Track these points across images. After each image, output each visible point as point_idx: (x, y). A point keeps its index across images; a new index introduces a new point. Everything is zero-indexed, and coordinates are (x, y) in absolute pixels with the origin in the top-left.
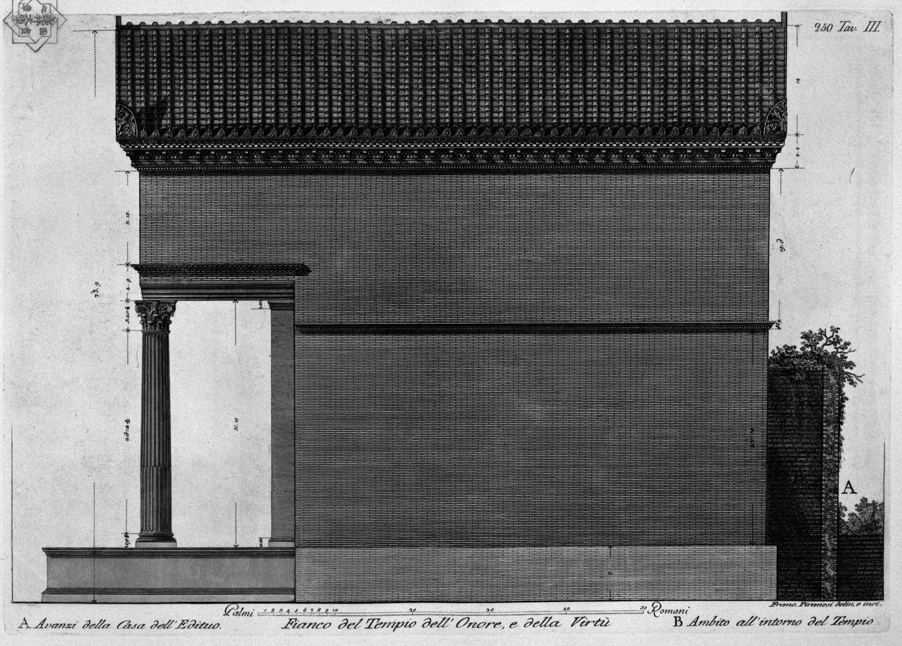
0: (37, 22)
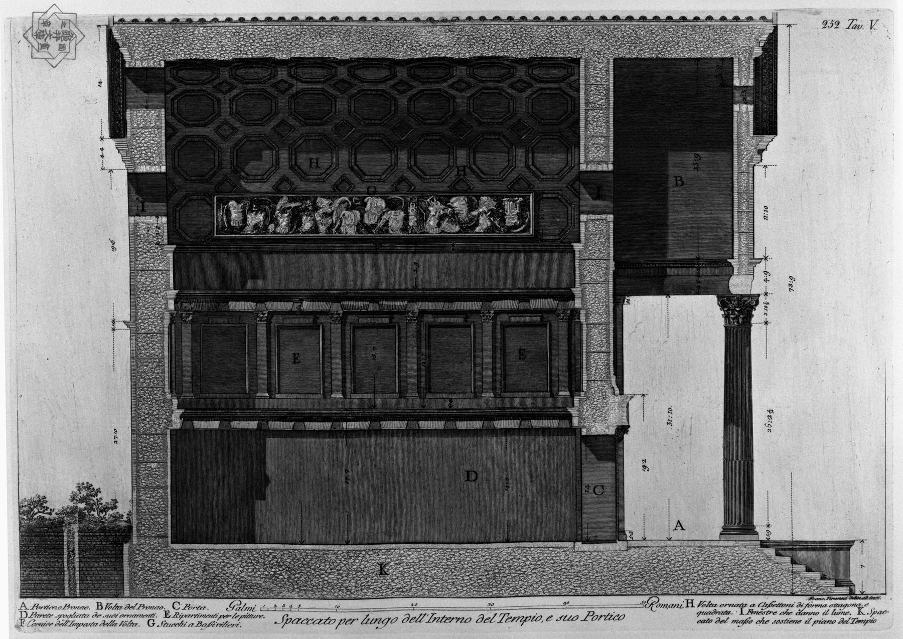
0: (56, 37)
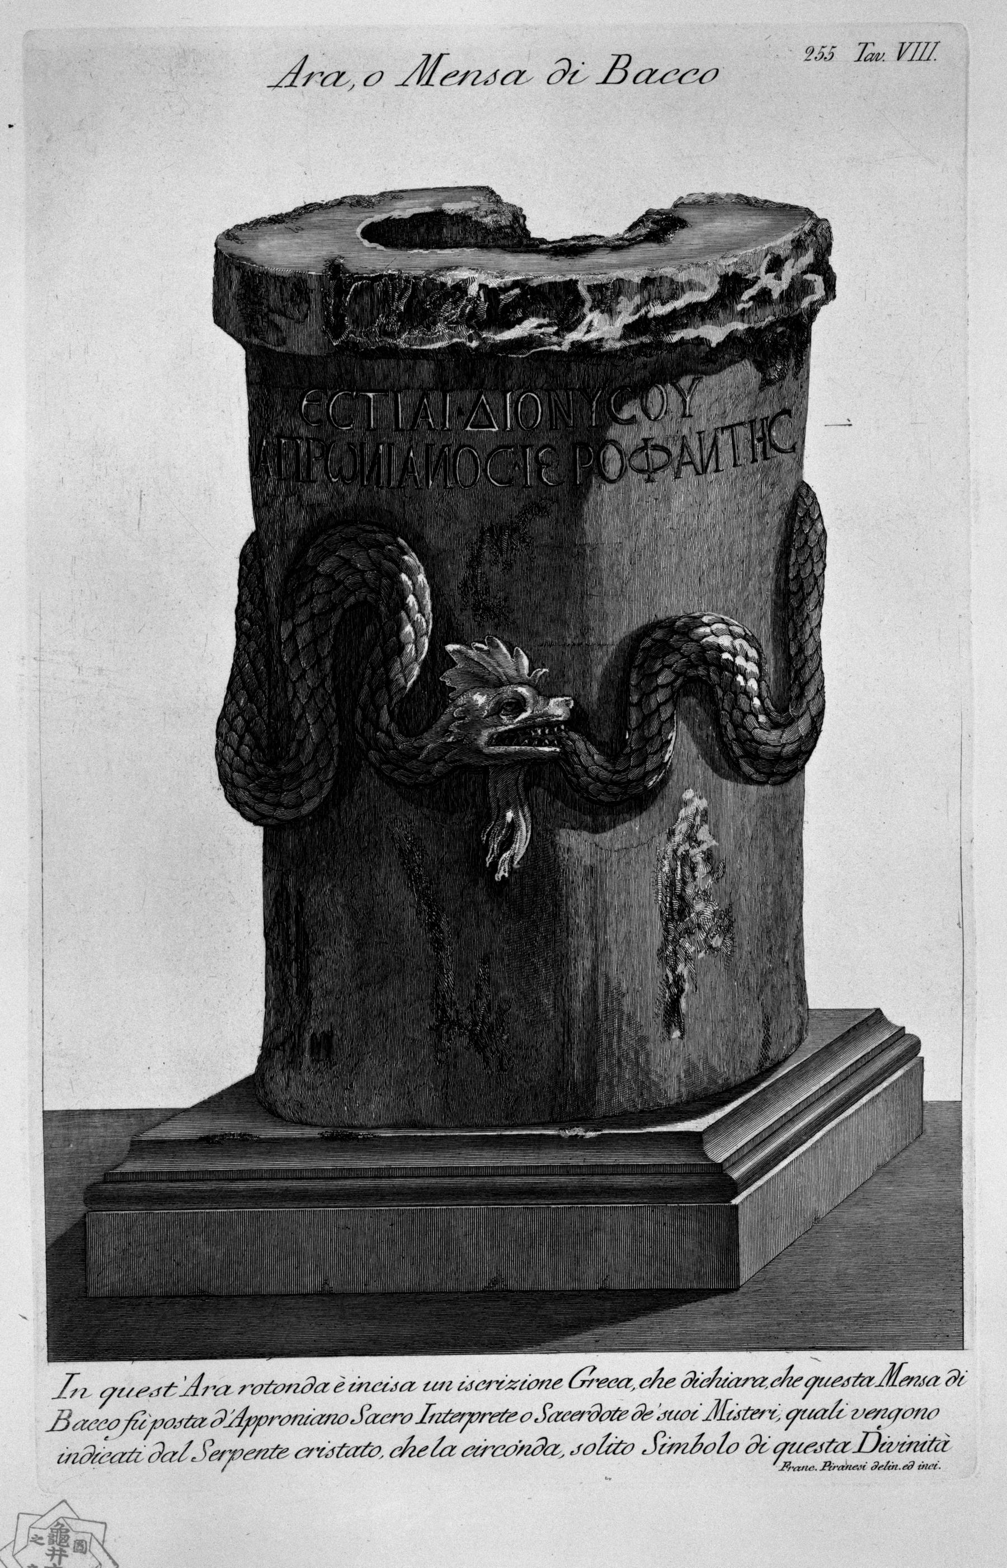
0: (60, 1556)
